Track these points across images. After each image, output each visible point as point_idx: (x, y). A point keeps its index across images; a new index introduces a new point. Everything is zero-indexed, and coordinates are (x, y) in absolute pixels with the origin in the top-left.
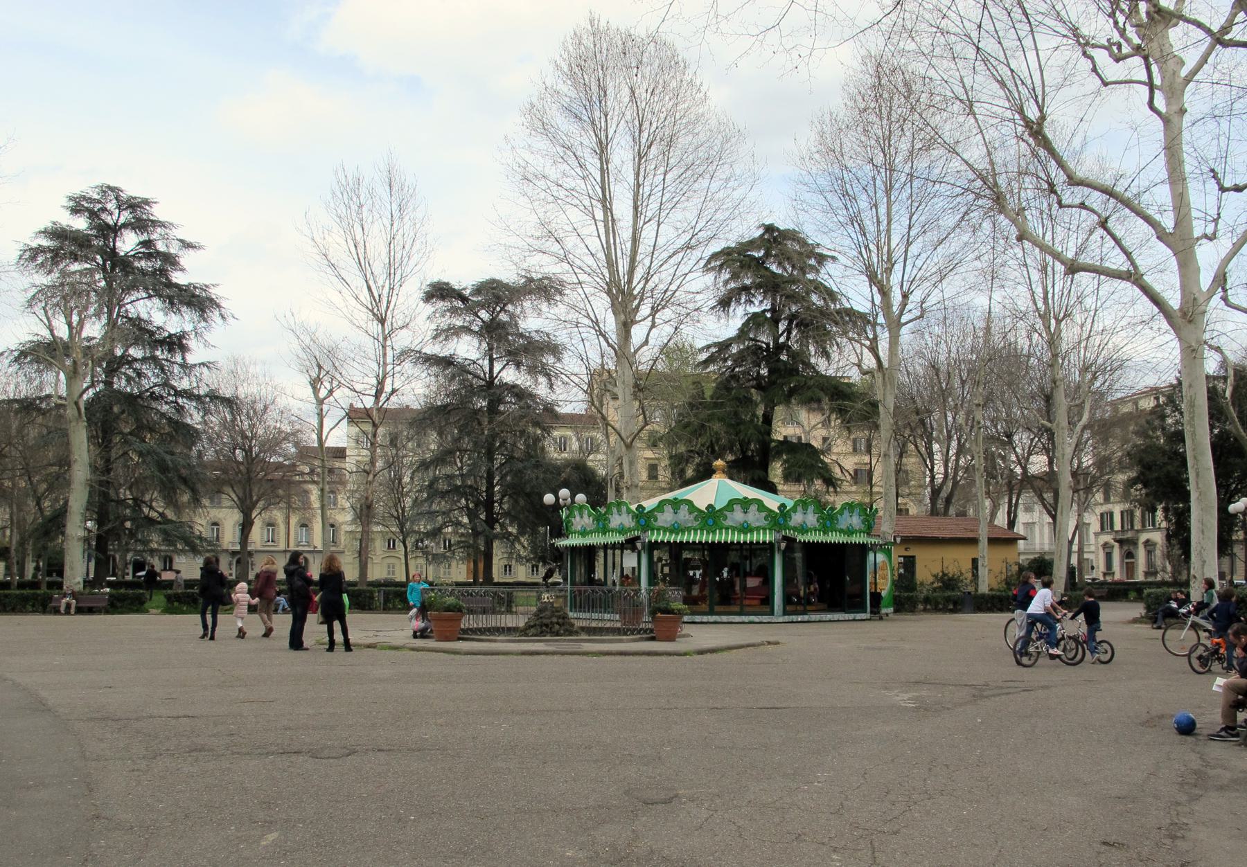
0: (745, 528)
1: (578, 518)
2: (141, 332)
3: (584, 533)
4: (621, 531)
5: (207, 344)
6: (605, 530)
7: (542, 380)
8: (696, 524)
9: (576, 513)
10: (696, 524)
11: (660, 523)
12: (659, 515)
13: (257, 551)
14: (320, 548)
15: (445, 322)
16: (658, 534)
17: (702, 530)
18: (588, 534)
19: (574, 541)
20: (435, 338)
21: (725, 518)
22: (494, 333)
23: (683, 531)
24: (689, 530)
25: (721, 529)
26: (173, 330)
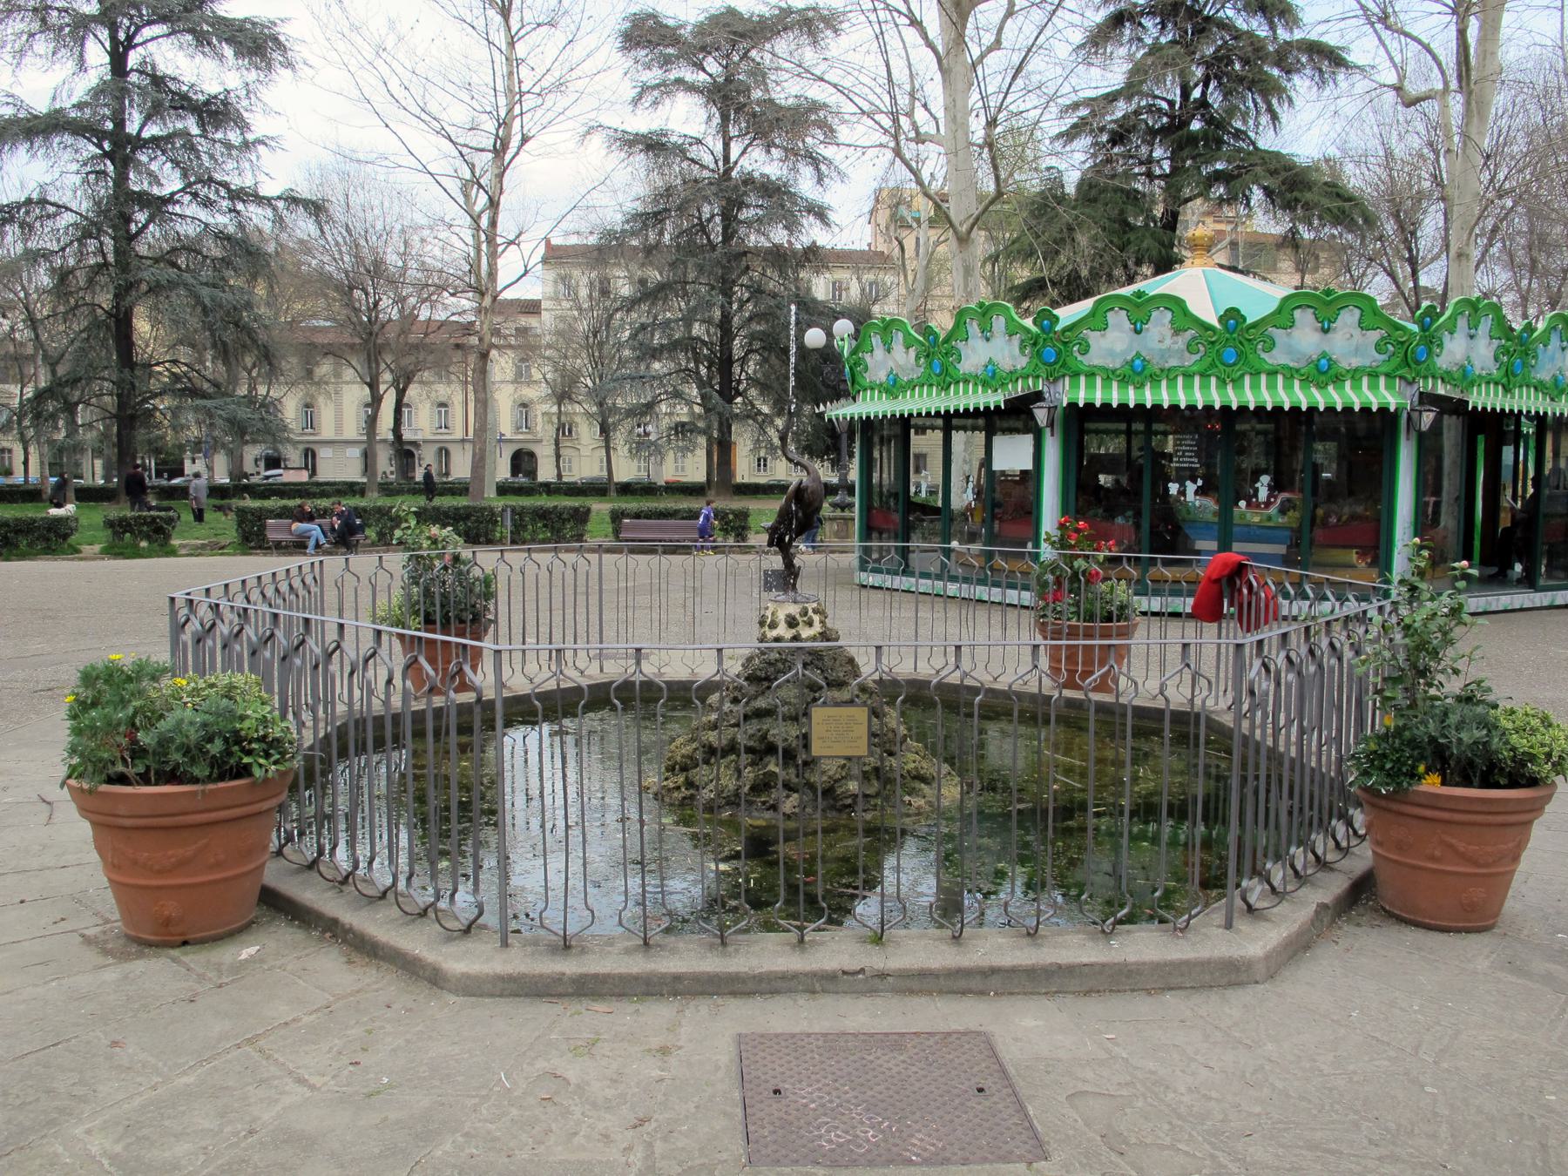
0: (1324, 372)
1: (879, 353)
2: (166, 96)
3: (893, 388)
4: (991, 378)
5: (267, 111)
6: (946, 380)
7: (807, 171)
8: (1190, 360)
9: (876, 341)
10: (1190, 360)
11: (1095, 358)
12: (1093, 337)
13: (425, 441)
14: (508, 436)
15: (654, 75)
16: (1091, 386)
17: (1204, 375)
18: (903, 389)
19: (870, 406)
20: (636, 101)
21: (1271, 345)
22: (727, 98)
23: (1154, 379)
24: (1169, 374)
25: (1256, 374)
26: (212, 88)
